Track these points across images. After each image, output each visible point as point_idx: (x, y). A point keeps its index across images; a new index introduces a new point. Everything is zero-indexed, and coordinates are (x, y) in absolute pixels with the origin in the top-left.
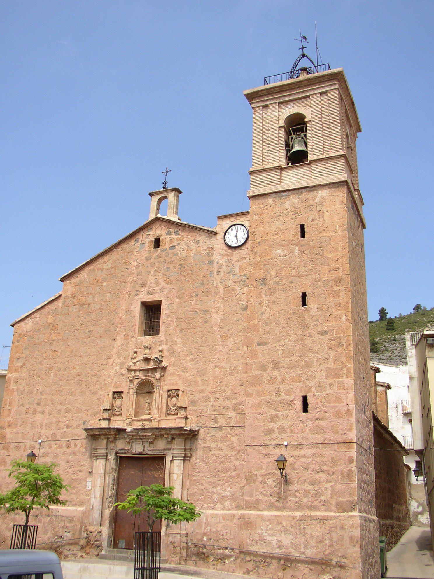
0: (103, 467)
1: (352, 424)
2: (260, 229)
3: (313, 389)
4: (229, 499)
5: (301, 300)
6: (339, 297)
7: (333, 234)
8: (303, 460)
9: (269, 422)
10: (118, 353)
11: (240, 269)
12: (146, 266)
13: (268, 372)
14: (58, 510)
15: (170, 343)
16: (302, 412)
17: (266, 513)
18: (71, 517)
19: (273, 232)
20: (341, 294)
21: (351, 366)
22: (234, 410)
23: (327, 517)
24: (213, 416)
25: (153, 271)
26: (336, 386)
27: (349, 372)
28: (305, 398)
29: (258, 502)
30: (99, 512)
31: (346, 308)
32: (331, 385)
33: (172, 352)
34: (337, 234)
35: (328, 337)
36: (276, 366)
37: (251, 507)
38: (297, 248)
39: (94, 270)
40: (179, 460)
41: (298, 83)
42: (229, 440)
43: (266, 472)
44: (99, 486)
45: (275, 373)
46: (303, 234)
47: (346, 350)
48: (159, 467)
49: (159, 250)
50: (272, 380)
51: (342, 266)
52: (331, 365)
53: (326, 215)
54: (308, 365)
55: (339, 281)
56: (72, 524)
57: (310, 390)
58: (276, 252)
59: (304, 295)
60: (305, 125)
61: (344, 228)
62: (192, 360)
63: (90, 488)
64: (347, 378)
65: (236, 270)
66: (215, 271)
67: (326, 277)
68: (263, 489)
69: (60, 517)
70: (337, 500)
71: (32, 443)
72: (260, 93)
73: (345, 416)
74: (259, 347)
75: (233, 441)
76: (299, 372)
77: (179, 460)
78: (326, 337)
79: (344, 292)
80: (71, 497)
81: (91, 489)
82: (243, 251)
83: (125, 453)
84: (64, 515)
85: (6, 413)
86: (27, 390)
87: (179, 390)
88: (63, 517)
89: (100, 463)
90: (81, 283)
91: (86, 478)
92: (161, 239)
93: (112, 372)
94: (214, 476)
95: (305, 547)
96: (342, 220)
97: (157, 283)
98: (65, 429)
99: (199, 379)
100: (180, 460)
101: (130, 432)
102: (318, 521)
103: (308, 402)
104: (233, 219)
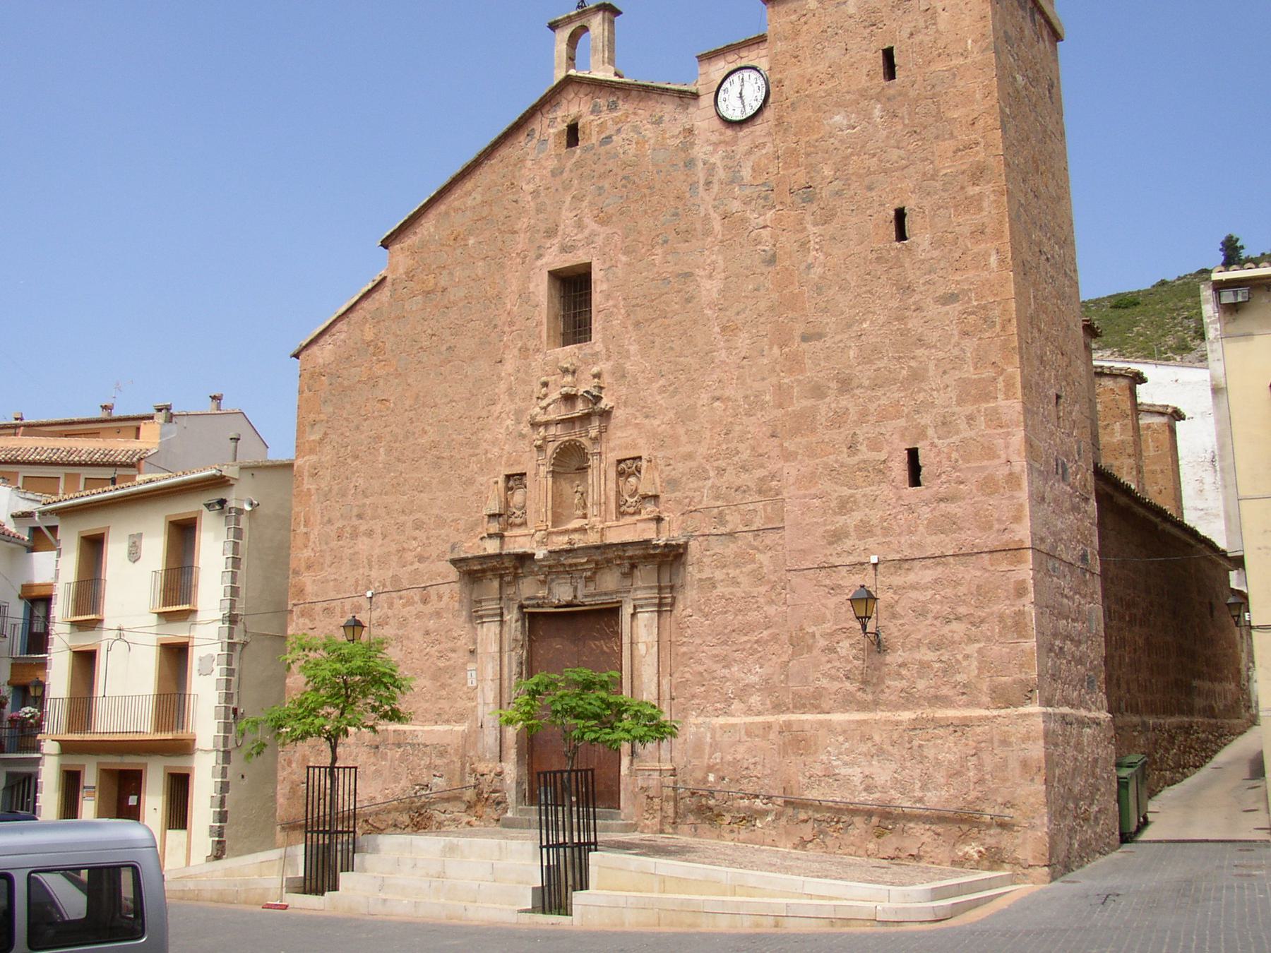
4: (758, 690)
24: (716, 510)
40: (647, 612)
42: (753, 561)
62: (663, 390)
63: (475, 684)
69: (421, 746)
77: (647, 612)
81: (477, 688)
83: (539, 606)
84: (428, 743)
87: (640, 458)
89: (489, 630)
94: (725, 643)
100: (651, 611)
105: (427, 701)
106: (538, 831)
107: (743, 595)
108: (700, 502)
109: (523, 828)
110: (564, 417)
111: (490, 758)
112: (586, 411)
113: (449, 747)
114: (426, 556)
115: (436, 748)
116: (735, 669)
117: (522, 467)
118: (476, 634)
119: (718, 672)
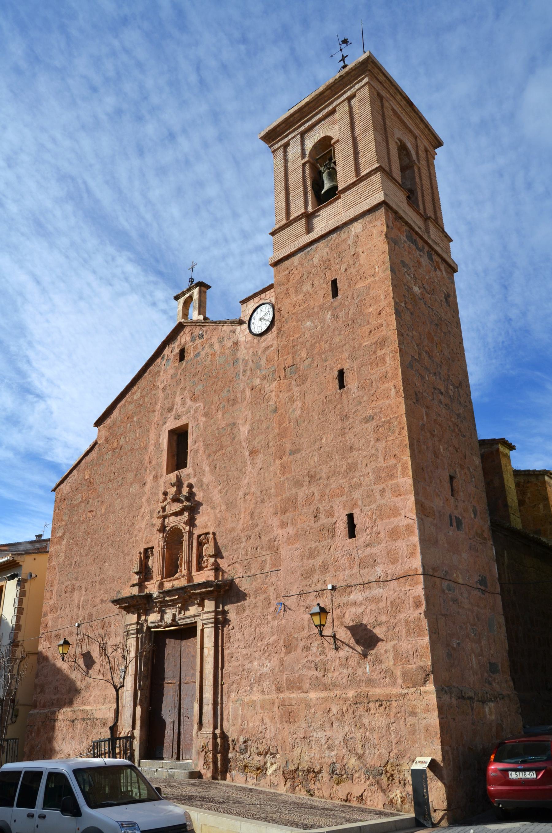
1: (415, 545)
2: (287, 301)
3: (360, 503)
5: (337, 382)
6: (385, 363)
7: (373, 279)
8: (353, 610)
9: (308, 559)
10: (148, 501)
11: (267, 361)
12: (172, 385)
13: (304, 488)
15: (198, 475)
16: (347, 538)
17: (313, 695)
19: (301, 301)
20: (387, 359)
21: (407, 459)
22: (269, 548)
23: (390, 695)
24: (246, 562)
25: (179, 390)
26: (388, 493)
27: (404, 468)
28: (350, 517)
29: (300, 679)
31: (395, 376)
32: (382, 492)
33: (201, 484)
34: (377, 278)
35: (374, 423)
36: (312, 478)
37: (293, 688)
38: (330, 313)
39: (125, 405)
40: (209, 628)
41: (320, 97)
43: (309, 634)
45: (314, 489)
46: (335, 292)
47: (399, 436)
49: (184, 363)
50: (309, 500)
51: (385, 320)
52: (381, 463)
53: (363, 259)
54: (352, 468)
55: (382, 343)
57: (355, 505)
58: (305, 326)
59: (341, 373)
60: (332, 148)
61: (385, 267)
64: (403, 477)
65: (263, 362)
66: (241, 371)
67: (367, 341)
68: (306, 660)
70: (403, 668)
71: (70, 628)
72: (278, 129)
73: (404, 534)
76: (341, 481)
77: (209, 628)
78: (370, 426)
79: (391, 355)
82: (270, 336)
84: (98, 717)
85: (48, 595)
86: (66, 563)
90: (115, 423)
92: (185, 349)
93: (143, 524)
95: (363, 747)
96: (383, 256)
97: (184, 403)
99: (228, 515)
101: (156, 599)
102: (378, 704)
103: (355, 522)
104: (256, 299)
108: (238, 558)
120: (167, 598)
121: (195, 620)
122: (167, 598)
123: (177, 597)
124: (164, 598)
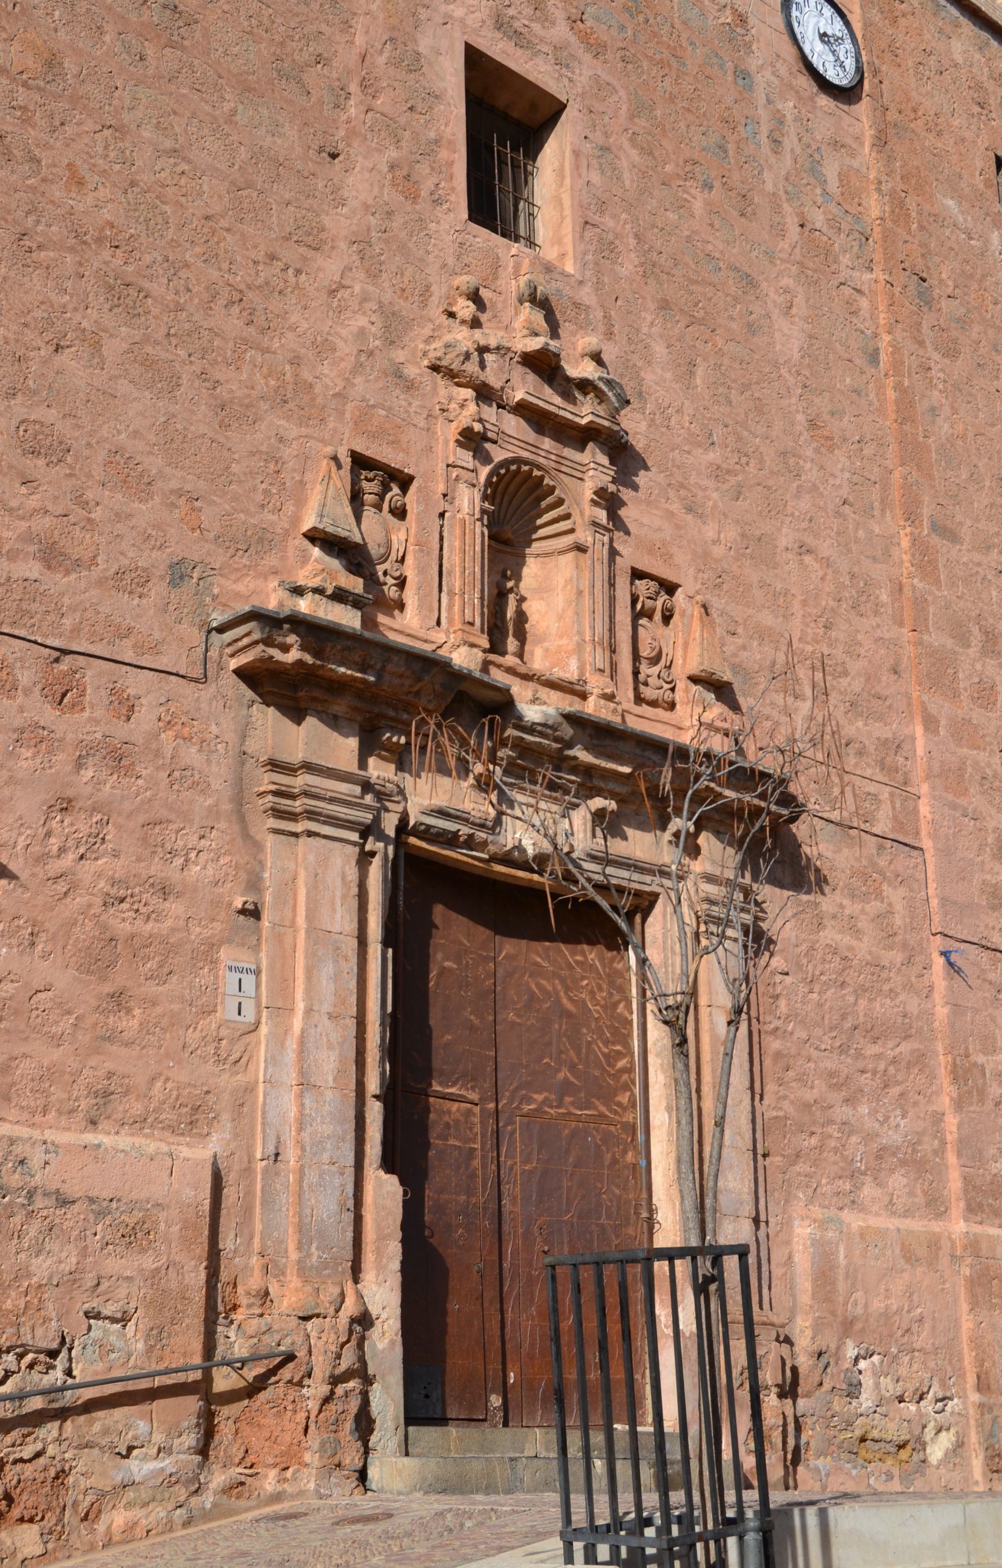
0: (344, 897)
4: (903, 1163)
14: (18, 1149)
18: (133, 1205)
30: (337, 1181)
42: (879, 896)
44: (330, 1016)
48: (579, 958)
56: (149, 1262)
63: (249, 1015)
69: (39, 1202)
74: (429, 376)
75: (890, 905)
80: (109, 1065)
81: (257, 1024)
83: (451, 840)
84: (73, 1189)
88: (64, 1202)
91: (212, 946)
94: (843, 1049)
98: (33, 569)
105: (57, 1040)
106: (555, 1497)
107: (869, 957)
109: (497, 1492)
110: (541, 404)
111: (325, 1265)
112: (606, 423)
113: (162, 1216)
114: (76, 553)
115: (101, 1214)
116: (864, 1109)
117: (401, 456)
118: (262, 864)
119: (837, 1110)
120: (582, 754)
121: (655, 888)
122: (582, 754)
123: (626, 770)
124: (570, 745)
